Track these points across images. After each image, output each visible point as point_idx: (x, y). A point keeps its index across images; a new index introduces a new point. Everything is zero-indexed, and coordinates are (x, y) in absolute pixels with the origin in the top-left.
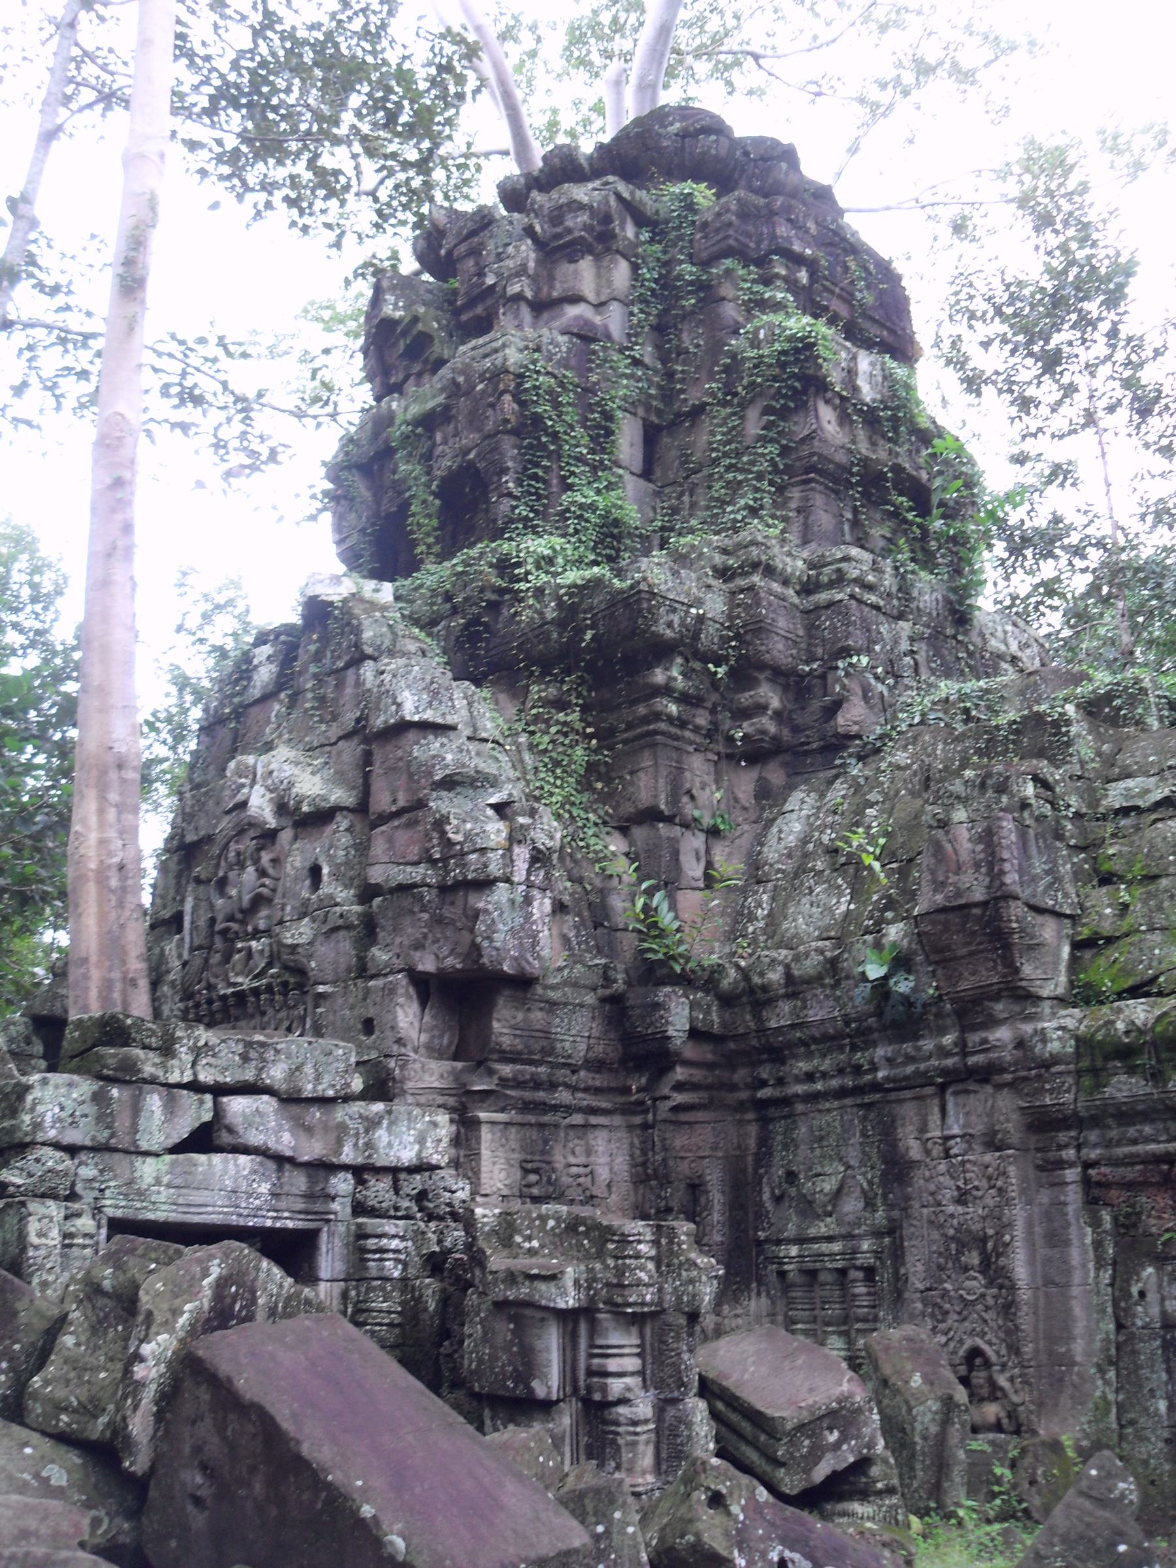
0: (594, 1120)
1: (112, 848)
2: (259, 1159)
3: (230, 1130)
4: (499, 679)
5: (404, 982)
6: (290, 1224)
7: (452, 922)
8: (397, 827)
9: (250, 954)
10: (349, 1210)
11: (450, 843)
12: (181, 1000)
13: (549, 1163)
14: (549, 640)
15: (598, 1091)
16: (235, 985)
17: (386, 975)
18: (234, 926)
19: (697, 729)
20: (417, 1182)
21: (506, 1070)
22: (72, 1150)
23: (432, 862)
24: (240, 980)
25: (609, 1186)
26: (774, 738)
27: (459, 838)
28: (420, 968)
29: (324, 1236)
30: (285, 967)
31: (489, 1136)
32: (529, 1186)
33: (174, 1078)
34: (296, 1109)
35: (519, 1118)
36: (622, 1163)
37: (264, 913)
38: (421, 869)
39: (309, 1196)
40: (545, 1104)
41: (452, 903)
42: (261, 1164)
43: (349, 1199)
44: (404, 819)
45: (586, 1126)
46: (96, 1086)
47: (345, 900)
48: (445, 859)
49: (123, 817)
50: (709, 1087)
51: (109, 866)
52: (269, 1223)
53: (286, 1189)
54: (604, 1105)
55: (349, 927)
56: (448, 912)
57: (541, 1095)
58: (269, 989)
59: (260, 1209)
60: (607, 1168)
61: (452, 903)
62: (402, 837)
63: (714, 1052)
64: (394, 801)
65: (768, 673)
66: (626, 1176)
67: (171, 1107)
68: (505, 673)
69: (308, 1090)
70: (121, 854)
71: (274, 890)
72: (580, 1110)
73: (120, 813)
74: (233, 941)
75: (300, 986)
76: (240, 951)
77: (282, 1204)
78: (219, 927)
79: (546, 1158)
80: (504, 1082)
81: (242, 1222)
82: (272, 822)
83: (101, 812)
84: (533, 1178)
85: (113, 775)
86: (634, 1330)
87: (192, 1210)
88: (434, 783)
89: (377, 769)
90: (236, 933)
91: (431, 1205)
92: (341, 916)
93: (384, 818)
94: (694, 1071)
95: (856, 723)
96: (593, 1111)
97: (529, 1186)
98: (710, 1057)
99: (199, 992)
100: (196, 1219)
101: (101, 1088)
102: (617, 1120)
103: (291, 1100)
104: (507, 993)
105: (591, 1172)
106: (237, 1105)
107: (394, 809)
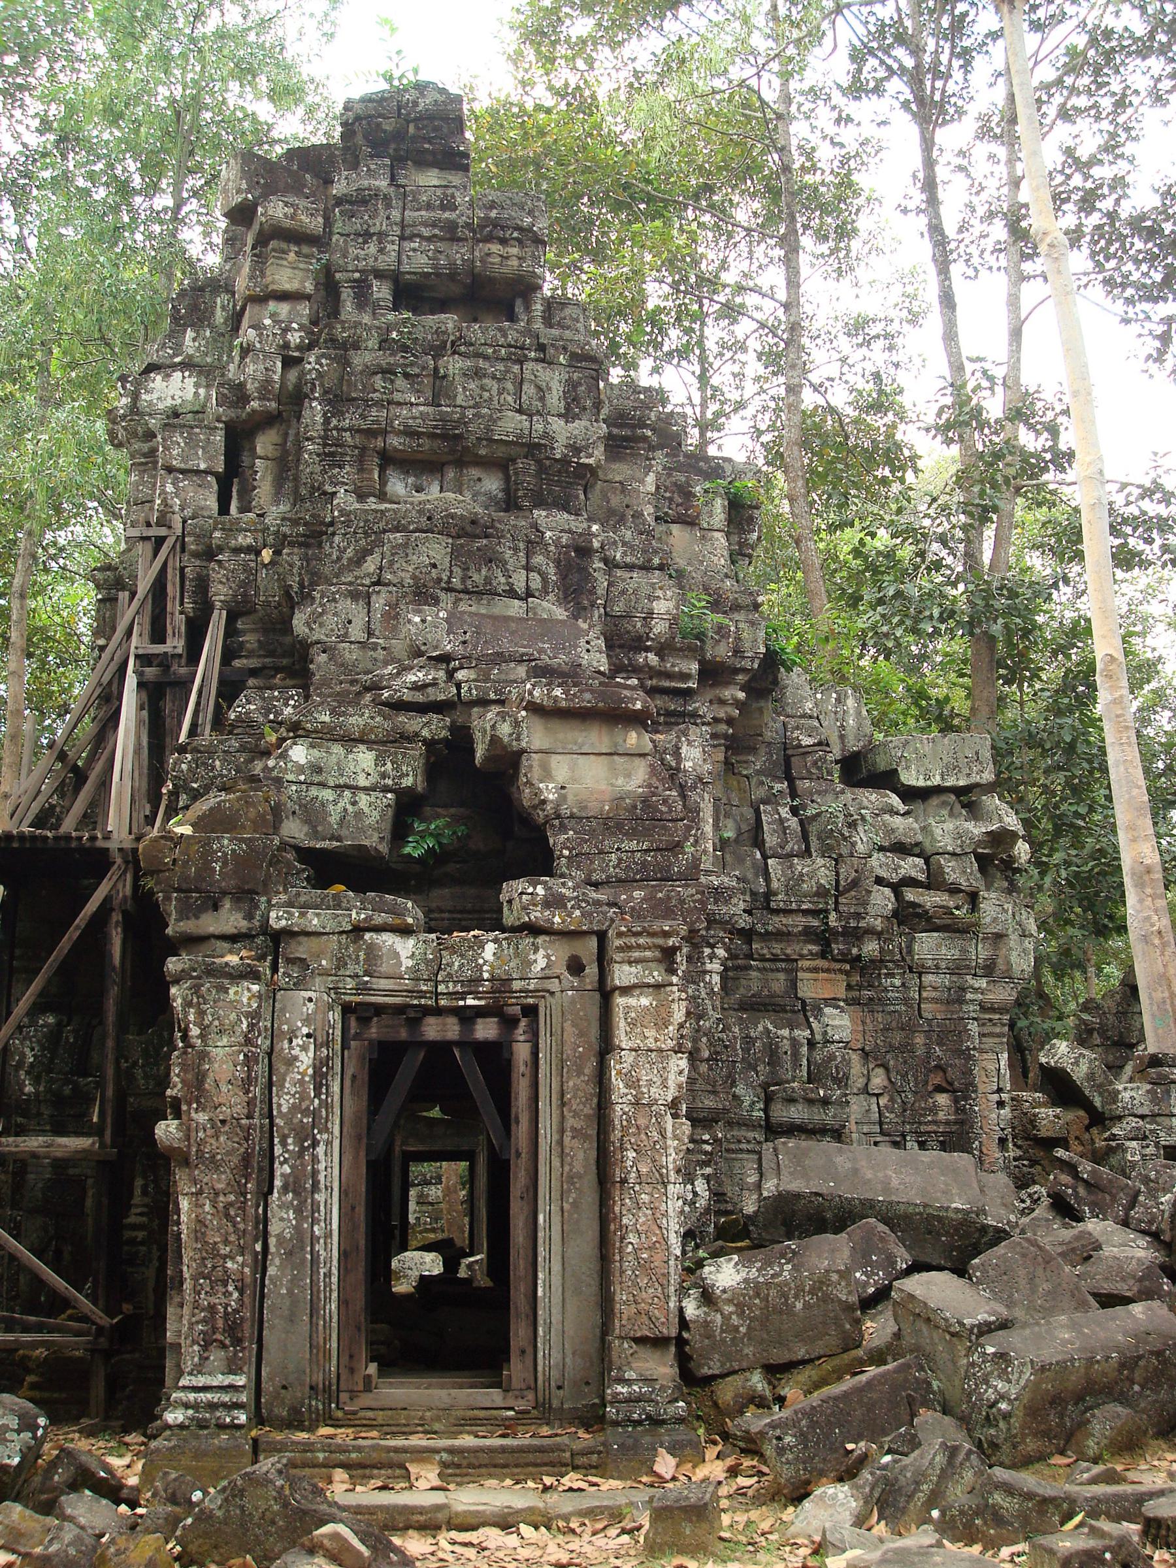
22: (1142, 1117)
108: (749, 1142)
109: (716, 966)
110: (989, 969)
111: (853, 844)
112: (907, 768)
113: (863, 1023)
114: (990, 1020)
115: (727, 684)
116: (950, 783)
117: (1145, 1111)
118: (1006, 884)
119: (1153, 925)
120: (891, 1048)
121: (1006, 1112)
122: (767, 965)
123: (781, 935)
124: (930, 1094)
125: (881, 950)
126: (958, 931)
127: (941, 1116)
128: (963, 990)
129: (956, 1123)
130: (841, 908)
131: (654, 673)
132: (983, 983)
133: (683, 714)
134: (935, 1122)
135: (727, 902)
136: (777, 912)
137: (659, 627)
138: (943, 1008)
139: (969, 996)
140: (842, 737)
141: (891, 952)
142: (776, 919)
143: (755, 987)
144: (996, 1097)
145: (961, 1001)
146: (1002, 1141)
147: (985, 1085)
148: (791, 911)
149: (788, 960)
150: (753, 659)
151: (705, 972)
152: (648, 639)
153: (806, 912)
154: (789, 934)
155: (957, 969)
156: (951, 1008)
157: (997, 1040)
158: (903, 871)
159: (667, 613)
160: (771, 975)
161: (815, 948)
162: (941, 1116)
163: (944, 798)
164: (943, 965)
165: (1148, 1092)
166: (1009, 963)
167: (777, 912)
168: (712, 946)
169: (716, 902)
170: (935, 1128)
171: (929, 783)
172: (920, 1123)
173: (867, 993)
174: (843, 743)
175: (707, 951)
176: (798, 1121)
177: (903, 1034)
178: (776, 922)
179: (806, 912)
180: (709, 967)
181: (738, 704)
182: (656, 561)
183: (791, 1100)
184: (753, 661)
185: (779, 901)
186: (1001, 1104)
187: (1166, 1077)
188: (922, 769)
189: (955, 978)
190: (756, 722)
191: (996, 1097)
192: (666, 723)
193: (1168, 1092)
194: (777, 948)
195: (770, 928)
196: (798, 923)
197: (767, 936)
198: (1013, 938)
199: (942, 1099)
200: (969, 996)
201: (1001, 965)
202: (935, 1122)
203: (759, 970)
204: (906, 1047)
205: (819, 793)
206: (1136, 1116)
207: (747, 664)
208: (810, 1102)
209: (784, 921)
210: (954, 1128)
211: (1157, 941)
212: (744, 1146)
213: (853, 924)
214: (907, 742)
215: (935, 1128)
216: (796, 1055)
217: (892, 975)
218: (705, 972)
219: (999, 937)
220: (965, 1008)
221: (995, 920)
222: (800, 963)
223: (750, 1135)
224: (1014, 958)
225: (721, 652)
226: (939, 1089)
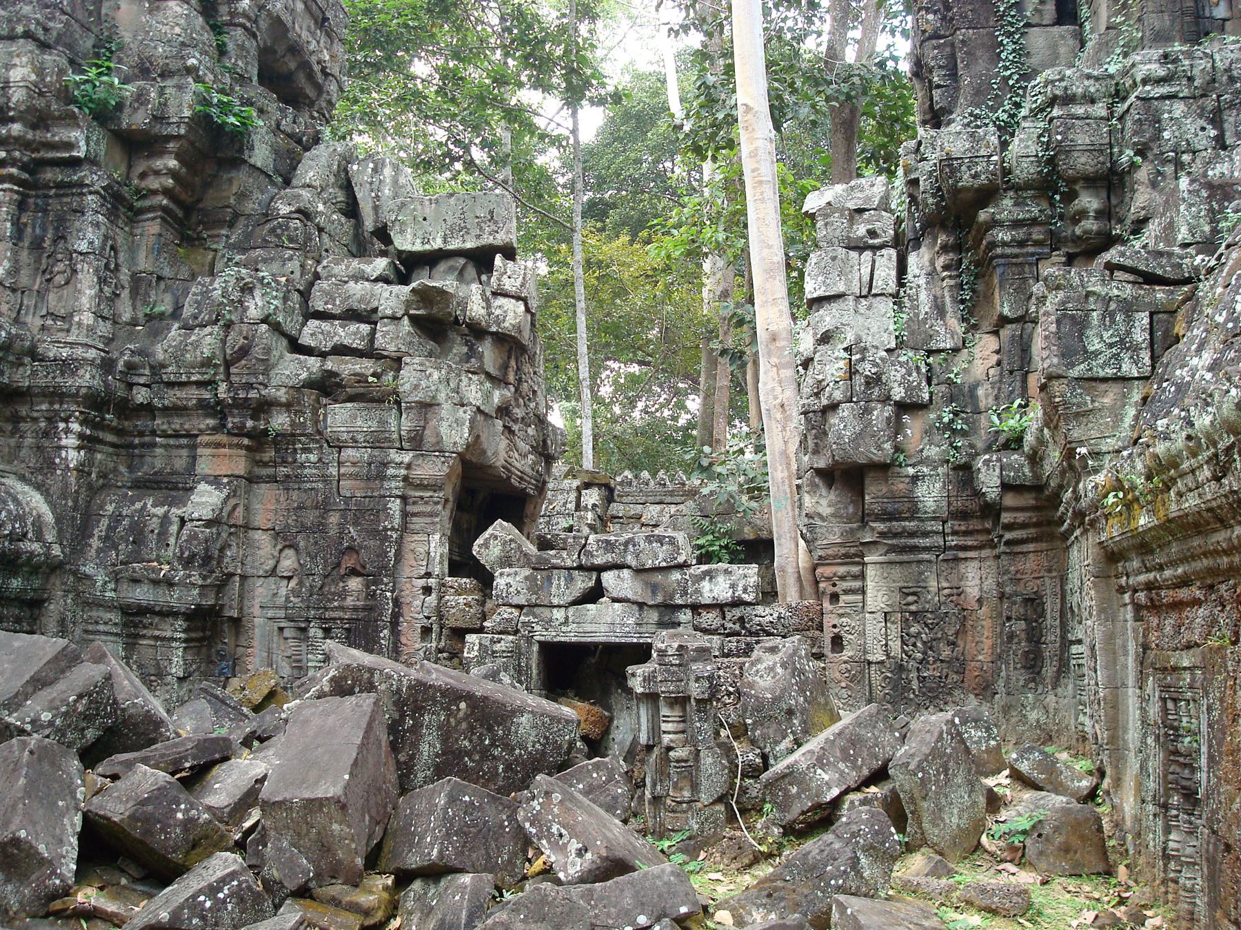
19: (1037, 243)
21: (881, 526)
22: (520, 607)
26: (1099, 233)
31: (873, 573)
32: (908, 604)
33: (569, 563)
34: (645, 576)
35: (882, 559)
36: (990, 583)
45: (957, 559)
50: (1036, 525)
54: (970, 543)
63: (1036, 499)
65: (1081, 183)
67: (570, 580)
69: (649, 564)
70: (780, 397)
77: (643, 630)
81: (617, 640)
84: (911, 599)
86: (677, 708)
94: (1028, 514)
95: (1143, 208)
97: (908, 604)
98: (1032, 502)
100: (589, 640)
103: (640, 571)
104: (872, 475)
106: (608, 578)
108: (106, 623)
109: (71, 441)
110: (416, 442)
111: (245, 309)
112: (402, 232)
113: (278, 501)
114: (422, 498)
115: (162, 153)
116: (454, 245)
117: (521, 600)
118: (465, 349)
119: (776, 398)
120: (303, 529)
121: (432, 599)
122: (172, 441)
123: (177, 410)
124: (343, 578)
125: (293, 424)
126: (372, 400)
127: (350, 601)
128: (385, 465)
129: (364, 609)
130: (234, 379)
131: (26, 145)
132: (407, 457)
133: (71, 185)
134: (341, 608)
135: (73, 373)
136: (171, 385)
137: (17, 95)
138: (362, 485)
139: (390, 472)
140: (376, 208)
141: (304, 425)
142: (171, 392)
143: (159, 464)
144: (422, 582)
145: (382, 477)
146: (426, 631)
147: (411, 570)
148: (182, 385)
149: (188, 435)
150: (178, 124)
151: (60, 448)
152: (10, 109)
153: (199, 384)
154: (185, 408)
155: (378, 441)
156: (371, 485)
157: (428, 520)
158: (336, 338)
159: (23, 80)
160: (175, 452)
161: (211, 422)
162: (350, 601)
163: (451, 262)
164: (360, 438)
165: (526, 578)
166: (438, 435)
167: (171, 385)
168: (66, 420)
169: (62, 374)
170: (341, 614)
171: (427, 247)
172: (326, 609)
173: (283, 470)
174: (376, 213)
175: (62, 425)
176: (144, 603)
177: (317, 513)
178: (172, 397)
179: (199, 384)
180: (64, 442)
181: (172, 173)
182: (20, 29)
183: (136, 581)
184: (178, 127)
185: (170, 373)
186: (427, 590)
187: (547, 561)
188: (420, 233)
189: (376, 452)
190: (225, 194)
191: (422, 582)
192: (57, 196)
193: (549, 579)
194: (177, 423)
195: (166, 402)
196: (192, 395)
197: (167, 411)
198: (446, 410)
199: (355, 584)
200: (390, 472)
201: (429, 437)
202: (341, 608)
203: (162, 446)
204: (321, 527)
205: (265, 261)
206: (511, 606)
207: (173, 130)
208: (156, 583)
209: (178, 394)
210: (361, 615)
211: (779, 416)
212: (101, 628)
213: (242, 395)
214: (403, 205)
215: (341, 614)
216: (163, 534)
217: (309, 451)
218: (60, 448)
219: (427, 406)
220: (386, 484)
221: (416, 387)
222: (199, 439)
223: (108, 616)
224: (444, 430)
225: (137, 119)
226: (354, 572)
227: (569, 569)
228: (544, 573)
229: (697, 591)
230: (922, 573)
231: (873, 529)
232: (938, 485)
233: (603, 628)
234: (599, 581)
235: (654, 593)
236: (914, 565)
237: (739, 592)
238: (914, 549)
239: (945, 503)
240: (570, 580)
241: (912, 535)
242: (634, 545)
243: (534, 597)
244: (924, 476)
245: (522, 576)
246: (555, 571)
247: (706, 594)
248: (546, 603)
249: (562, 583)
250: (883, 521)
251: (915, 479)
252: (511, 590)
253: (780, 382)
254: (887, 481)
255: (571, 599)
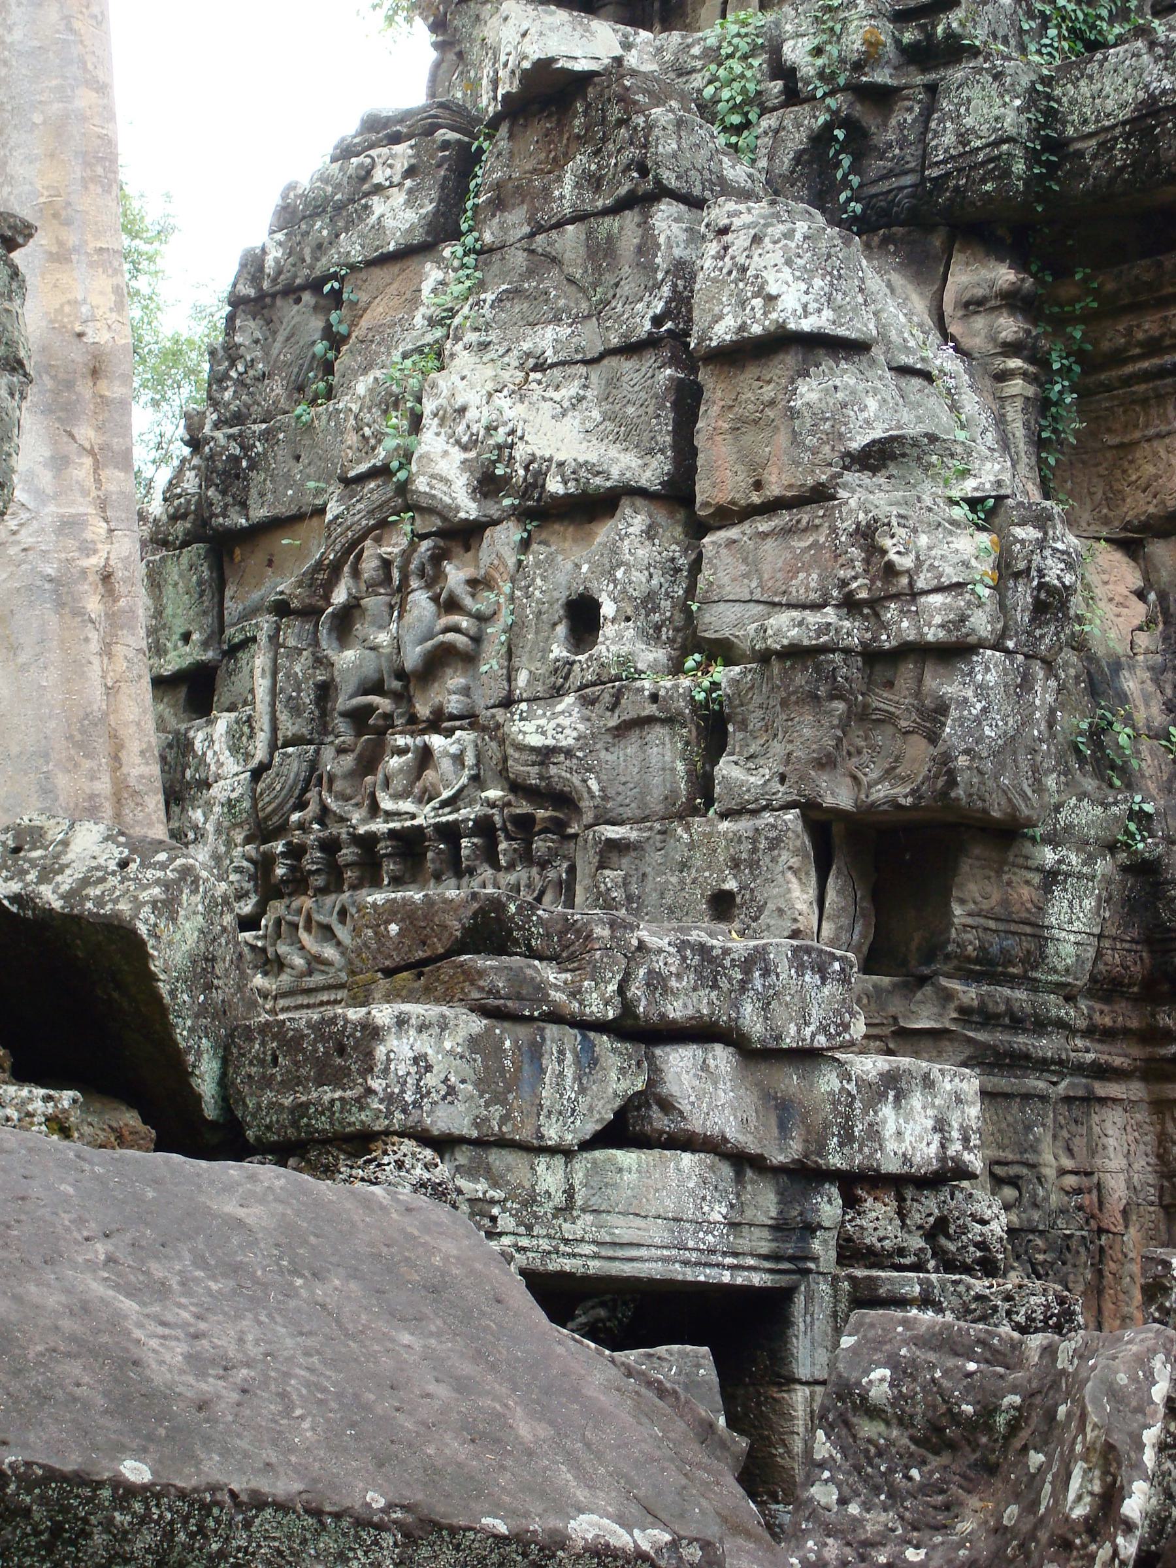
0: (1102, 1089)
1: (88, 535)
2: (708, 1159)
3: (667, 1105)
4: (885, 241)
5: (799, 826)
6: (757, 1279)
7: (890, 719)
8: (765, 535)
9: (426, 756)
10: (833, 1254)
11: (890, 570)
12: (248, 840)
13: (1032, 1166)
14: (1007, 173)
15: (1106, 1035)
16: (390, 815)
17: (755, 813)
18: (384, 704)
20: (928, 1207)
21: (969, 994)
23: (850, 605)
24: (407, 806)
25: (1125, 1213)
27: (907, 562)
28: (829, 801)
29: (800, 1300)
30: (516, 787)
34: (764, 1071)
37: (455, 680)
38: (830, 615)
39: (780, 1228)
40: (1027, 1057)
41: (890, 685)
42: (712, 1168)
43: (835, 1233)
44: (784, 518)
45: (1091, 1100)
46: (477, 1024)
47: (654, 667)
48: (875, 604)
49: (105, 474)
51: (84, 572)
52: (726, 1277)
53: (749, 1214)
54: (1118, 1061)
55: (670, 721)
56: (881, 701)
57: (1022, 1041)
58: (484, 827)
59: (712, 1252)
60: (1122, 1177)
61: (890, 685)
62: (773, 554)
64: (758, 485)
66: (1152, 1194)
67: (588, 1062)
68: (898, 230)
71: (477, 640)
72: (1079, 1069)
73: (97, 467)
74: (381, 732)
75: (558, 827)
76: (402, 751)
78: (343, 702)
79: (1030, 1157)
80: (965, 1012)
82: (469, 509)
83: (60, 463)
85: (85, 389)
87: (620, 1253)
88: (848, 454)
89: (711, 419)
90: (388, 716)
91: (952, 1247)
92: (654, 697)
93: (727, 516)
96: (1101, 1072)
99: (302, 826)
101: (488, 1030)
102: (1135, 1090)
104: (977, 851)
105: (1099, 1186)
107: (756, 499)
165: (474, 1043)
193: (535, 1052)
211: (93, 605)
227: (584, 1025)
228: (523, 1032)
229: (874, 1133)
230: (1028, 1128)
231: (947, 996)
232: (1089, 903)
233: (657, 1233)
234: (655, 1076)
235: (784, 1128)
236: (1015, 1105)
237: (955, 1148)
238: (1019, 1061)
239: (1091, 953)
240: (588, 1062)
241: (1016, 1022)
242: (766, 973)
243: (497, 1111)
244: (1067, 875)
245: (462, 1034)
246: (551, 1030)
247: (891, 1145)
248: (525, 1134)
249: (569, 1073)
250: (970, 977)
251: (1052, 877)
252: (430, 1080)
253: (103, 505)
254: (999, 872)
255: (590, 1128)
